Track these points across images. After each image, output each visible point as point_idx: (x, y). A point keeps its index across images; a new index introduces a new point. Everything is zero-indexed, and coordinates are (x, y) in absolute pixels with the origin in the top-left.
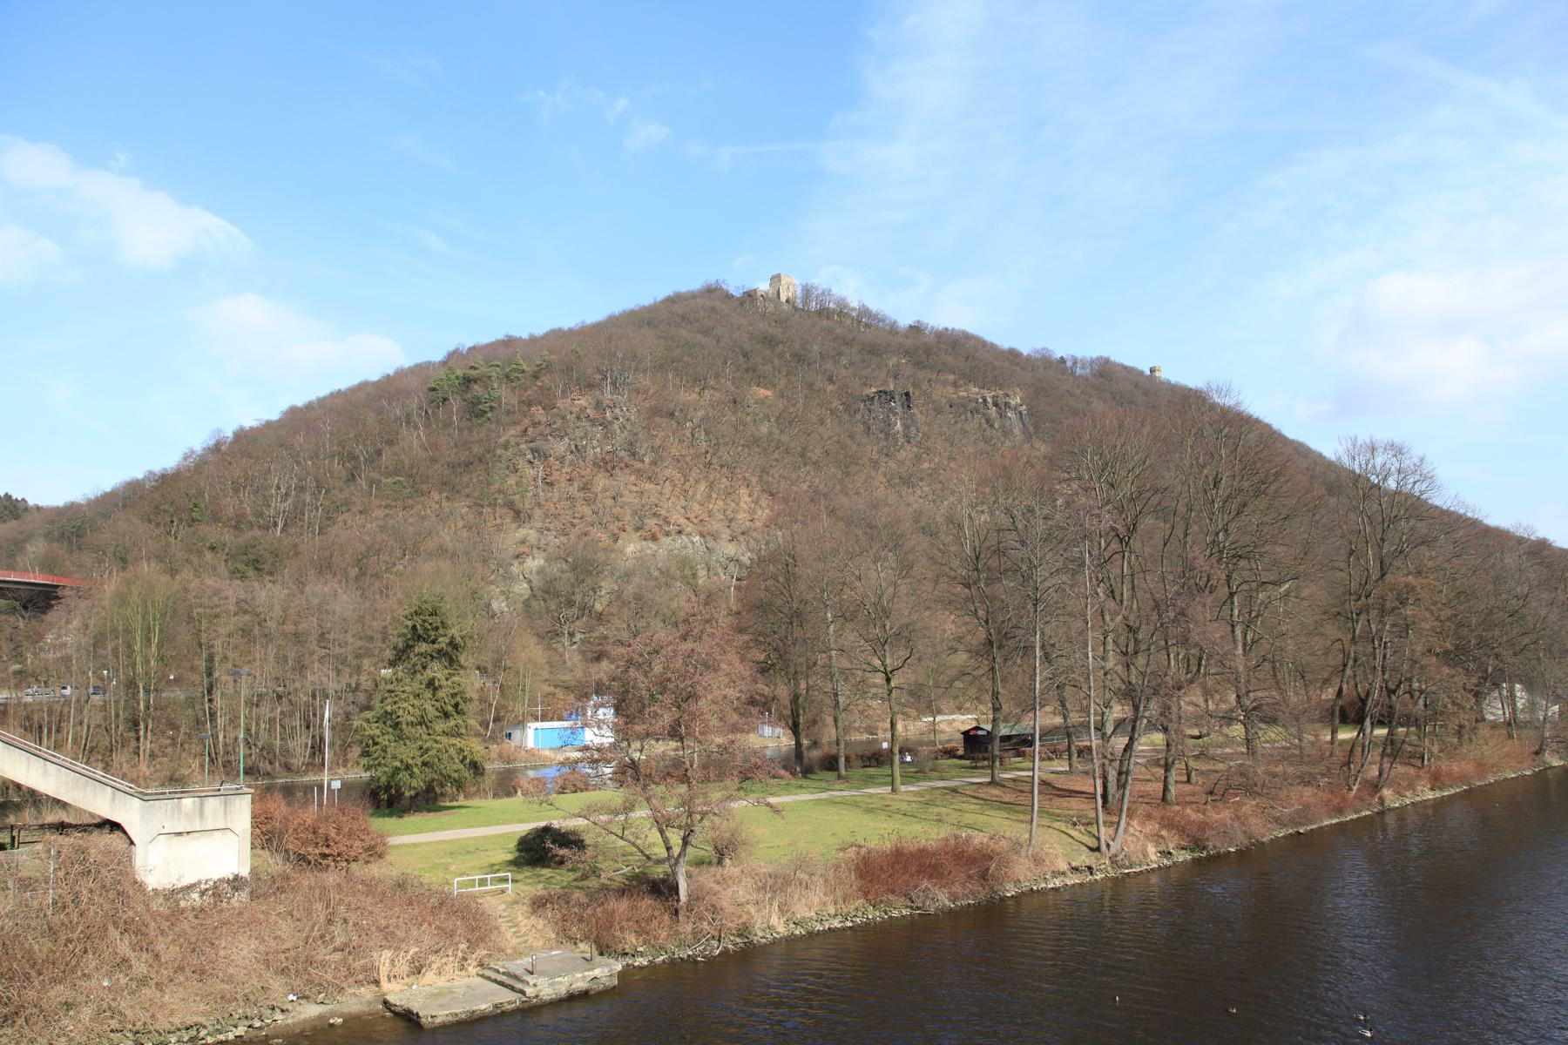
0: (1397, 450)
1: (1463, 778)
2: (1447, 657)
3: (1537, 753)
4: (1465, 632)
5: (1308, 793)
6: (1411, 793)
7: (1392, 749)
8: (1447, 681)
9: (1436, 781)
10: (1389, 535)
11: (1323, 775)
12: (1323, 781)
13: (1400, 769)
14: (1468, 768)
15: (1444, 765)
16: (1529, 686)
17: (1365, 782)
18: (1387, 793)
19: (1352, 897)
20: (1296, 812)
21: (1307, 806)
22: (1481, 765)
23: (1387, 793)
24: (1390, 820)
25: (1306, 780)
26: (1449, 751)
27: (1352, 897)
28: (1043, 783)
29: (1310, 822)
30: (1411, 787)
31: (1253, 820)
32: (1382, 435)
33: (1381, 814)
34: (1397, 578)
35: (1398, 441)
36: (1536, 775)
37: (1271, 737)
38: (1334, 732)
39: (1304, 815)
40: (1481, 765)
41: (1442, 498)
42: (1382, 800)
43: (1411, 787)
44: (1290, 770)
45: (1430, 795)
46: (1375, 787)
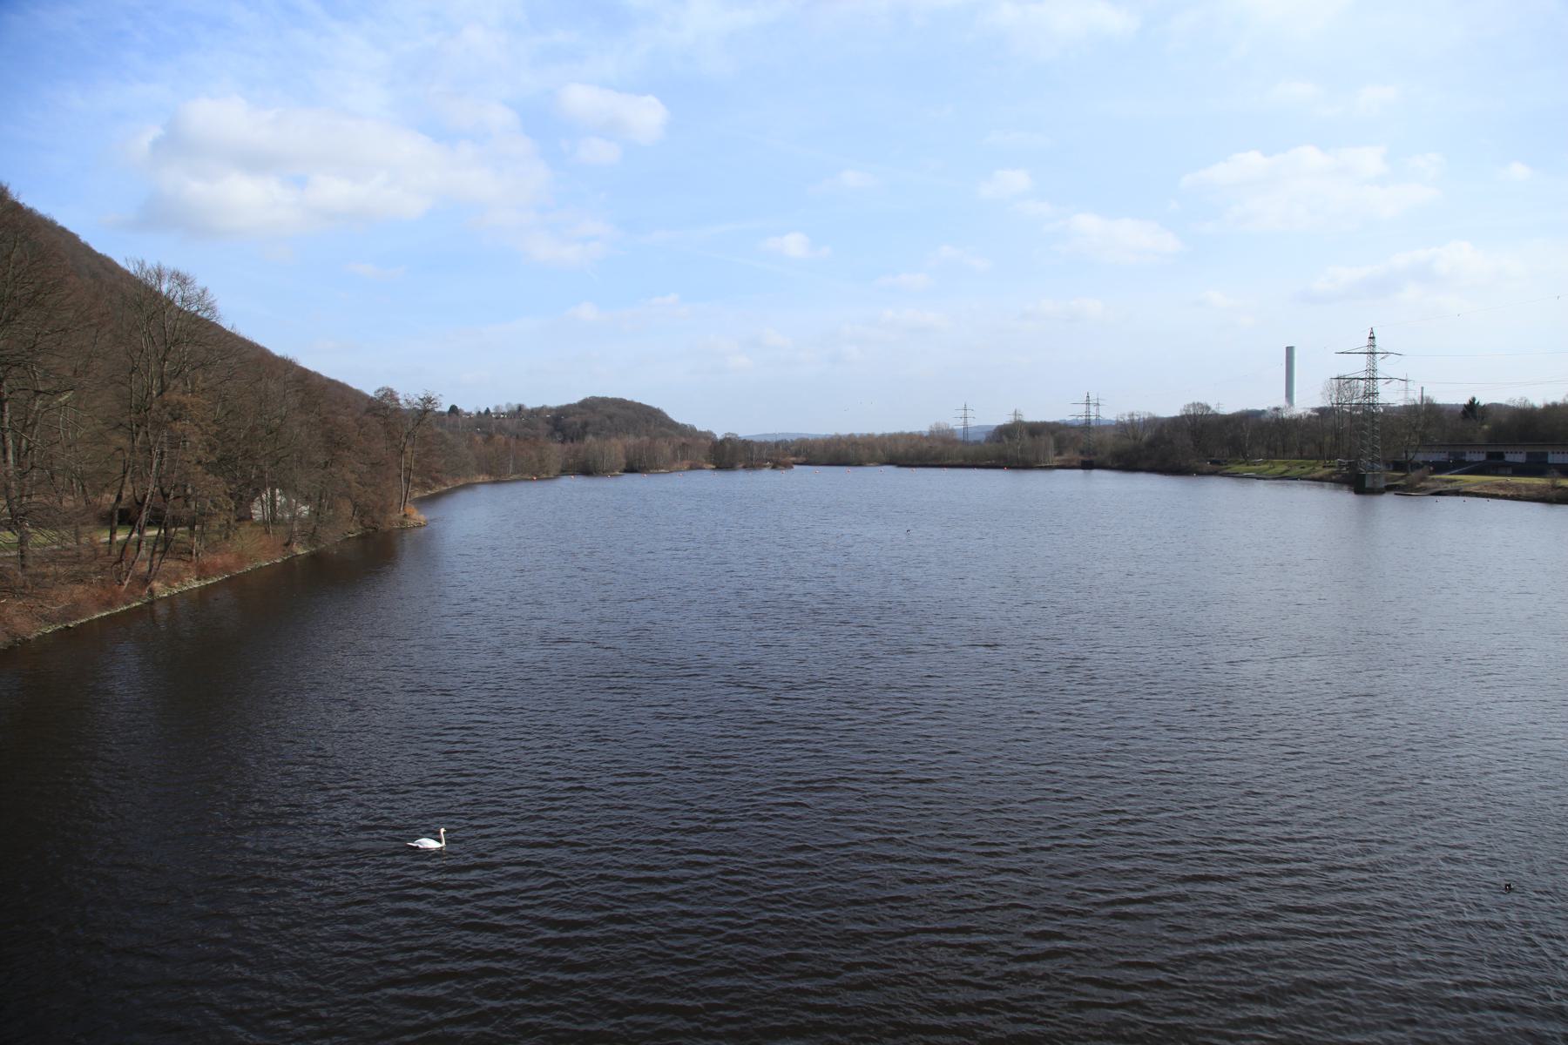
0: (183, 280)
1: (226, 569)
2: (211, 468)
3: (287, 545)
4: (231, 445)
5: (79, 590)
6: (178, 583)
7: (165, 547)
8: (214, 488)
9: (202, 573)
10: (170, 356)
11: (96, 573)
12: (95, 579)
13: (172, 564)
14: (230, 560)
15: (206, 559)
16: (284, 489)
17: (135, 578)
18: (156, 585)
19: (126, 678)
20: (65, 608)
21: (76, 603)
22: (241, 558)
23: (156, 585)
24: (161, 610)
25: (78, 579)
26: (212, 547)
27: (126, 678)
28: (1060, 454)
29: (80, 616)
30: (179, 578)
31: (17, 620)
32: (170, 263)
33: (151, 603)
34: (173, 397)
35: (183, 270)
36: (285, 562)
37: (40, 539)
38: (113, 534)
39: (75, 609)
40: (241, 558)
41: (226, 324)
42: (152, 591)
43: (179, 578)
44: (61, 570)
45: (196, 585)
46: (145, 581)
